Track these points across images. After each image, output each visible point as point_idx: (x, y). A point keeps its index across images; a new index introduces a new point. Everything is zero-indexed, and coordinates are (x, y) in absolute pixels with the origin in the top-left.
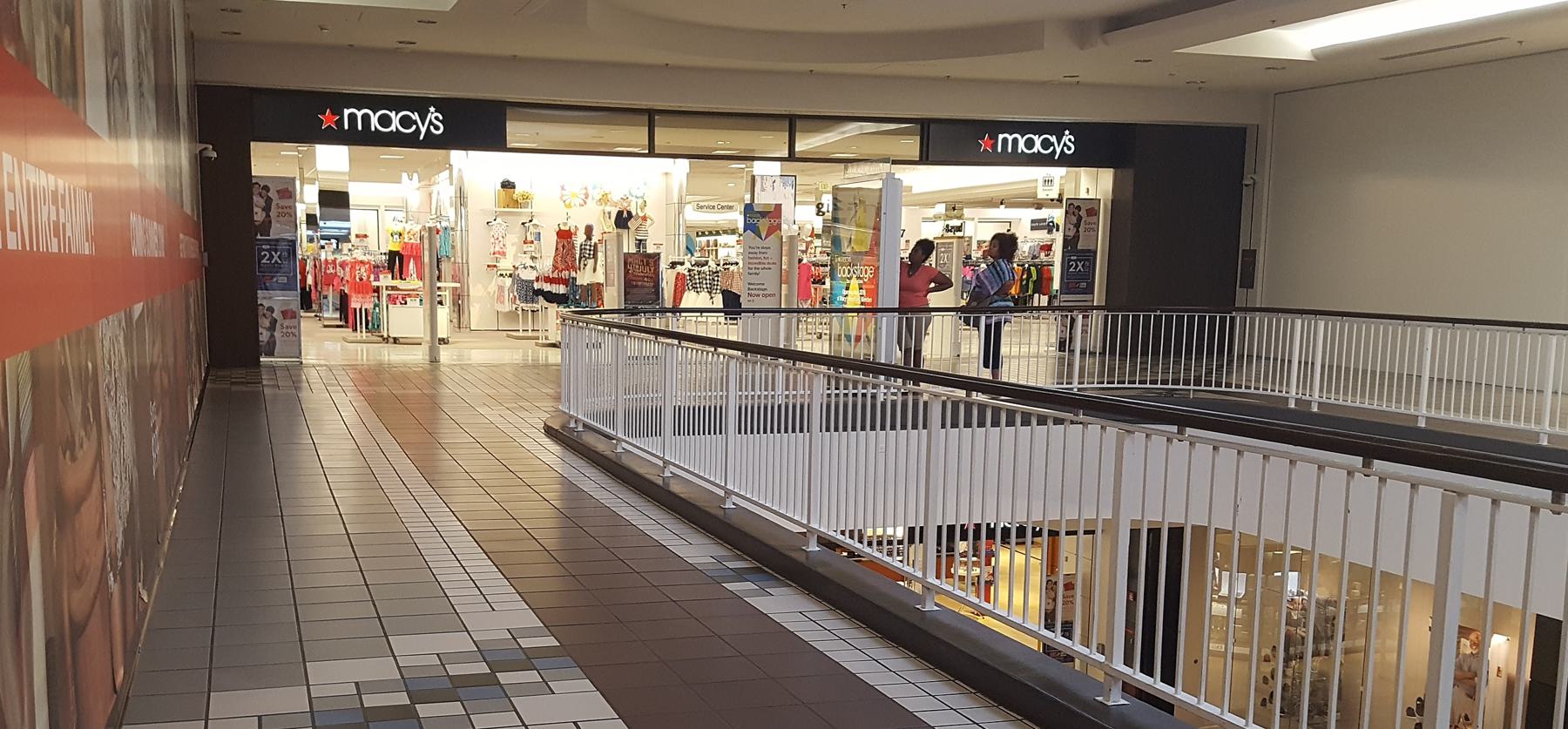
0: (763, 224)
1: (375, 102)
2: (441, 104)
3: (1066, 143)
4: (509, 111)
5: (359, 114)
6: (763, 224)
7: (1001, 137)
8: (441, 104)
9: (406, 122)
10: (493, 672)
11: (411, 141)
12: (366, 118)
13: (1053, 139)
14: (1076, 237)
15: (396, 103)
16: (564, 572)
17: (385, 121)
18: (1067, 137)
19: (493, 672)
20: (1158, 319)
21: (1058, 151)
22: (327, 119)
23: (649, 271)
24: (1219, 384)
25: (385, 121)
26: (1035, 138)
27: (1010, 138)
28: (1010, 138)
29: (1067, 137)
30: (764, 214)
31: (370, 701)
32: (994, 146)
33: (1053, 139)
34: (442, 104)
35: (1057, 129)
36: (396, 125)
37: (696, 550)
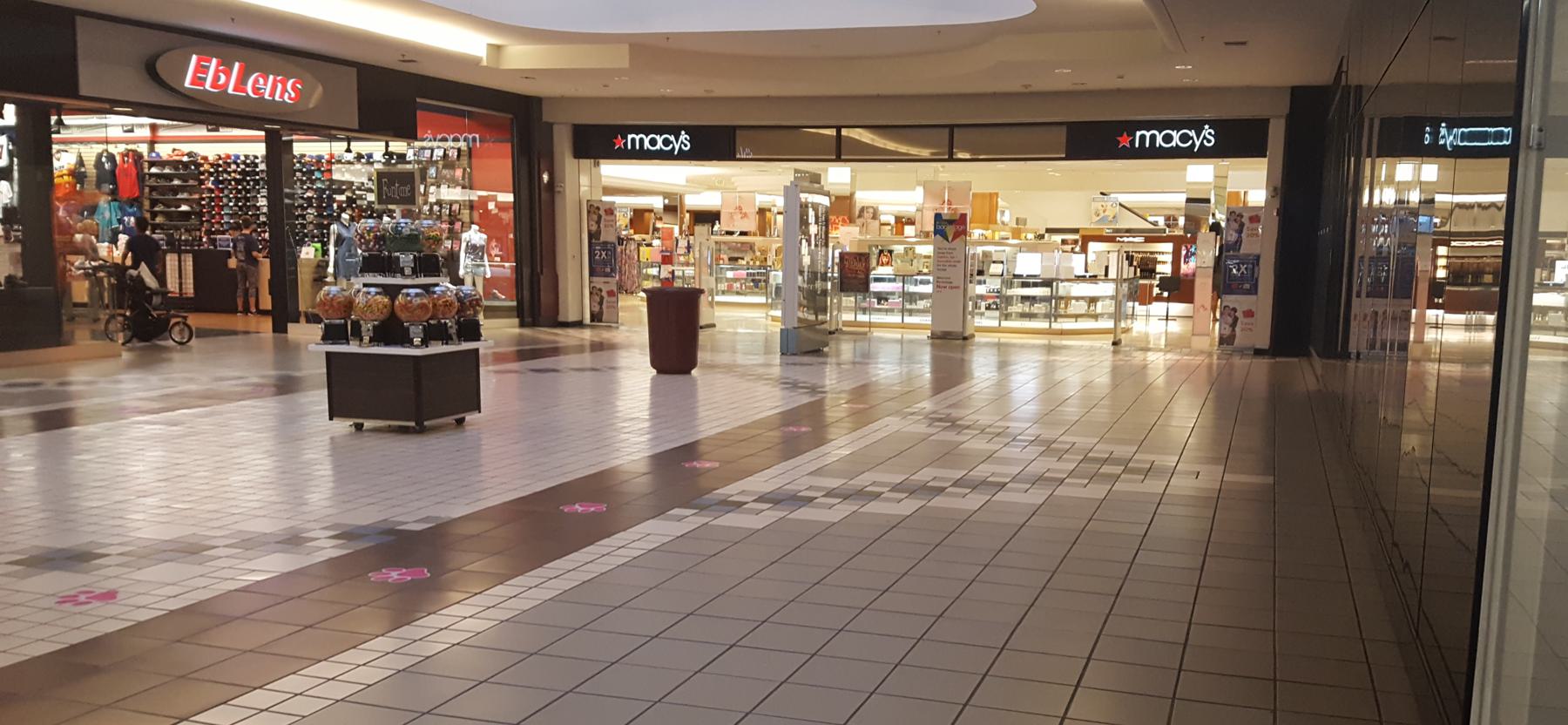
0: (950, 230)
1: (647, 130)
2: (688, 130)
3: (683, 141)
4: (1550, 113)
6: (950, 230)
7: (630, 137)
8: (688, 130)
9: (666, 142)
12: (1153, 137)
13: (672, 138)
14: (599, 232)
15: (660, 130)
17: (1168, 139)
18: (1207, 131)
21: (1198, 144)
22: (1124, 142)
23: (860, 266)
25: (1168, 139)
26: (1174, 133)
28: (1148, 134)
29: (1207, 131)
30: (951, 222)
32: (1132, 142)
33: (672, 138)
34: (689, 130)
36: (1176, 141)
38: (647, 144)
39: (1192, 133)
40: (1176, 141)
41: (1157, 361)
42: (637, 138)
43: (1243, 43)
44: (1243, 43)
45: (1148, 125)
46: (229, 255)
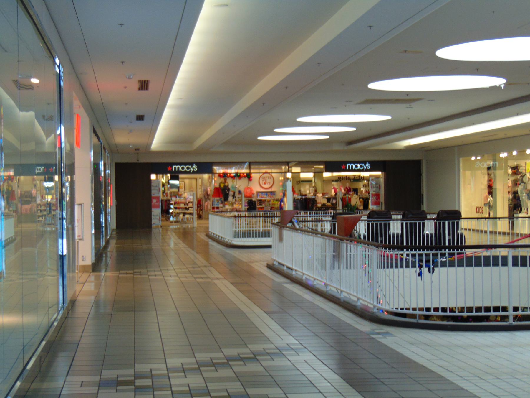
1: (180, 164)
2: (369, 162)
3: (195, 168)
5: (350, 165)
8: (369, 162)
9: (188, 168)
10: (228, 362)
11: (189, 173)
12: (178, 168)
15: (186, 164)
16: (25, 344)
17: (183, 168)
19: (228, 362)
20: (415, 224)
24: (420, 255)
25: (183, 168)
27: (350, 165)
29: (195, 166)
31: (120, 379)
32: (172, 169)
33: (363, 165)
34: (197, 164)
35: (191, 164)
37: (44, 343)
38: (180, 169)
39: (190, 167)
40: (185, 169)
41: (173, 273)
42: (177, 167)
43: (434, 100)
44: (434, 100)
45: (177, 164)
46: (172, 204)
